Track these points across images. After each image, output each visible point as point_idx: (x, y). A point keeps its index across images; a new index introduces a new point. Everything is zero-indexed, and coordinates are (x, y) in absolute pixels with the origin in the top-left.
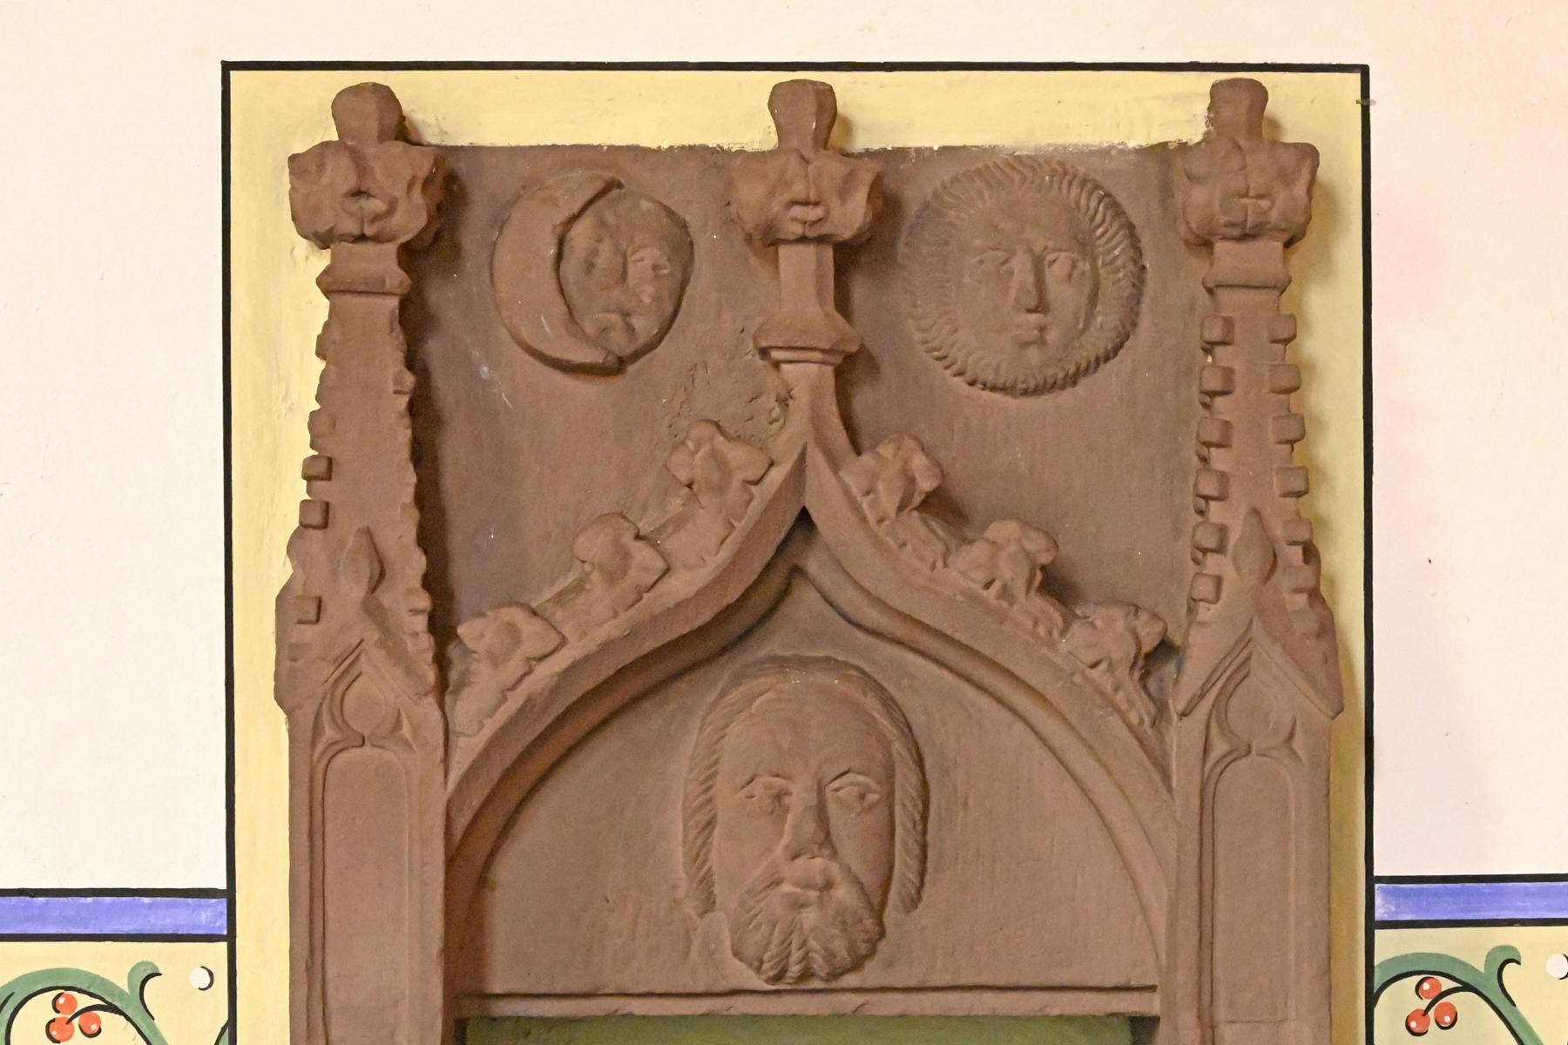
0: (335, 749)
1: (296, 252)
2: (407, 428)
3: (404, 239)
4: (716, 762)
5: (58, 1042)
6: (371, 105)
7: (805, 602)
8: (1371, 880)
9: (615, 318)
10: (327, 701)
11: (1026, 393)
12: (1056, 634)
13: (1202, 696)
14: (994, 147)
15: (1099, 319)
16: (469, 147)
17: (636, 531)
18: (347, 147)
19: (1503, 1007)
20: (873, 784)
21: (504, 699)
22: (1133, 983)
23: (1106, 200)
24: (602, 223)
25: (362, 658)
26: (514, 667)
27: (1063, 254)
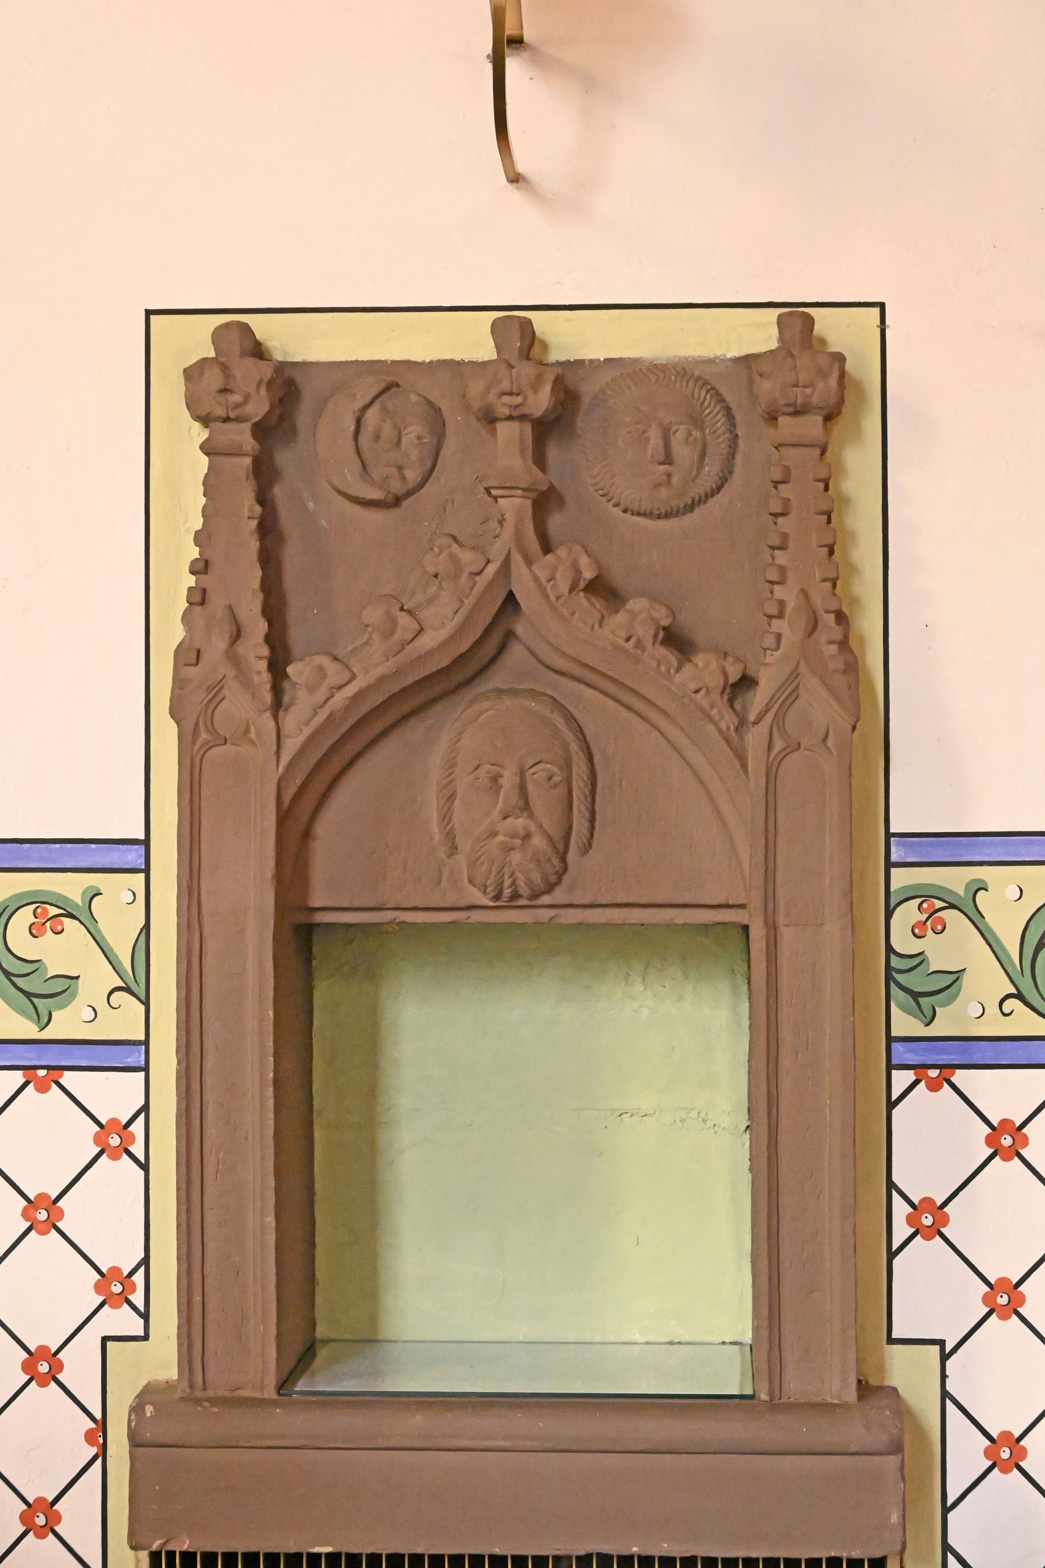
0: (208, 747)
1: (192, 430)
2: (257, 541)
3: (256, 419)
4: (455, 757)
5: (37, 937)
6: (235, 335)
7: (516, 653)
8: (888, 835)
9: (393, 470)
10: (203, 713)
11: (659, 517)
12: (672, 671)
13: (767, 711)
14: (640, 358)
15: (707, 468)
16: (302, 362)
17: (401, 605)
18: (220, 363)
19: (976, 919)
20: (555, 769)
21: (316, 713)
22: (731, 902)
23: (712, 392)
24: (384, 410)
25: (225, 688)
26: (321, 694)
27: (682, 427)
